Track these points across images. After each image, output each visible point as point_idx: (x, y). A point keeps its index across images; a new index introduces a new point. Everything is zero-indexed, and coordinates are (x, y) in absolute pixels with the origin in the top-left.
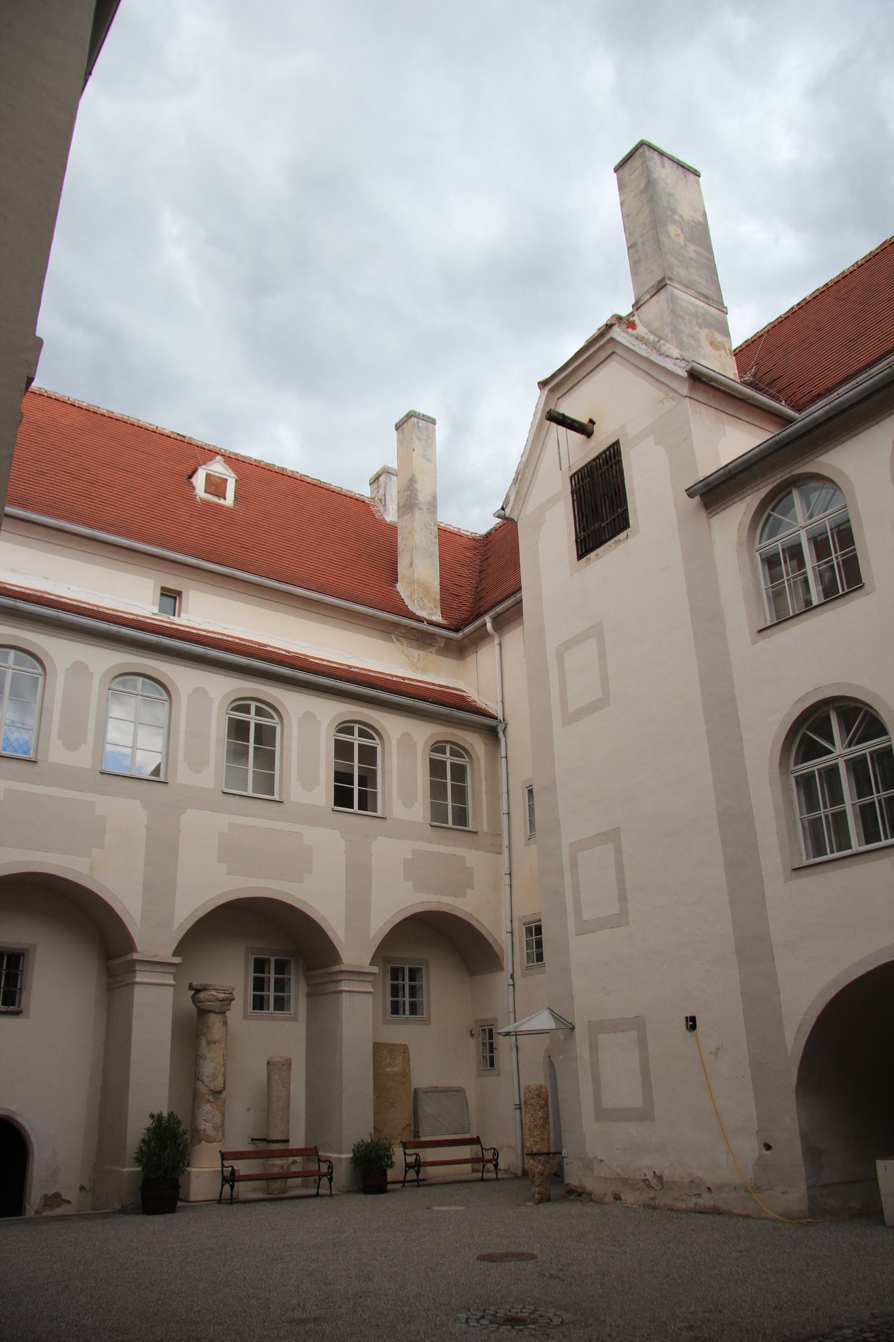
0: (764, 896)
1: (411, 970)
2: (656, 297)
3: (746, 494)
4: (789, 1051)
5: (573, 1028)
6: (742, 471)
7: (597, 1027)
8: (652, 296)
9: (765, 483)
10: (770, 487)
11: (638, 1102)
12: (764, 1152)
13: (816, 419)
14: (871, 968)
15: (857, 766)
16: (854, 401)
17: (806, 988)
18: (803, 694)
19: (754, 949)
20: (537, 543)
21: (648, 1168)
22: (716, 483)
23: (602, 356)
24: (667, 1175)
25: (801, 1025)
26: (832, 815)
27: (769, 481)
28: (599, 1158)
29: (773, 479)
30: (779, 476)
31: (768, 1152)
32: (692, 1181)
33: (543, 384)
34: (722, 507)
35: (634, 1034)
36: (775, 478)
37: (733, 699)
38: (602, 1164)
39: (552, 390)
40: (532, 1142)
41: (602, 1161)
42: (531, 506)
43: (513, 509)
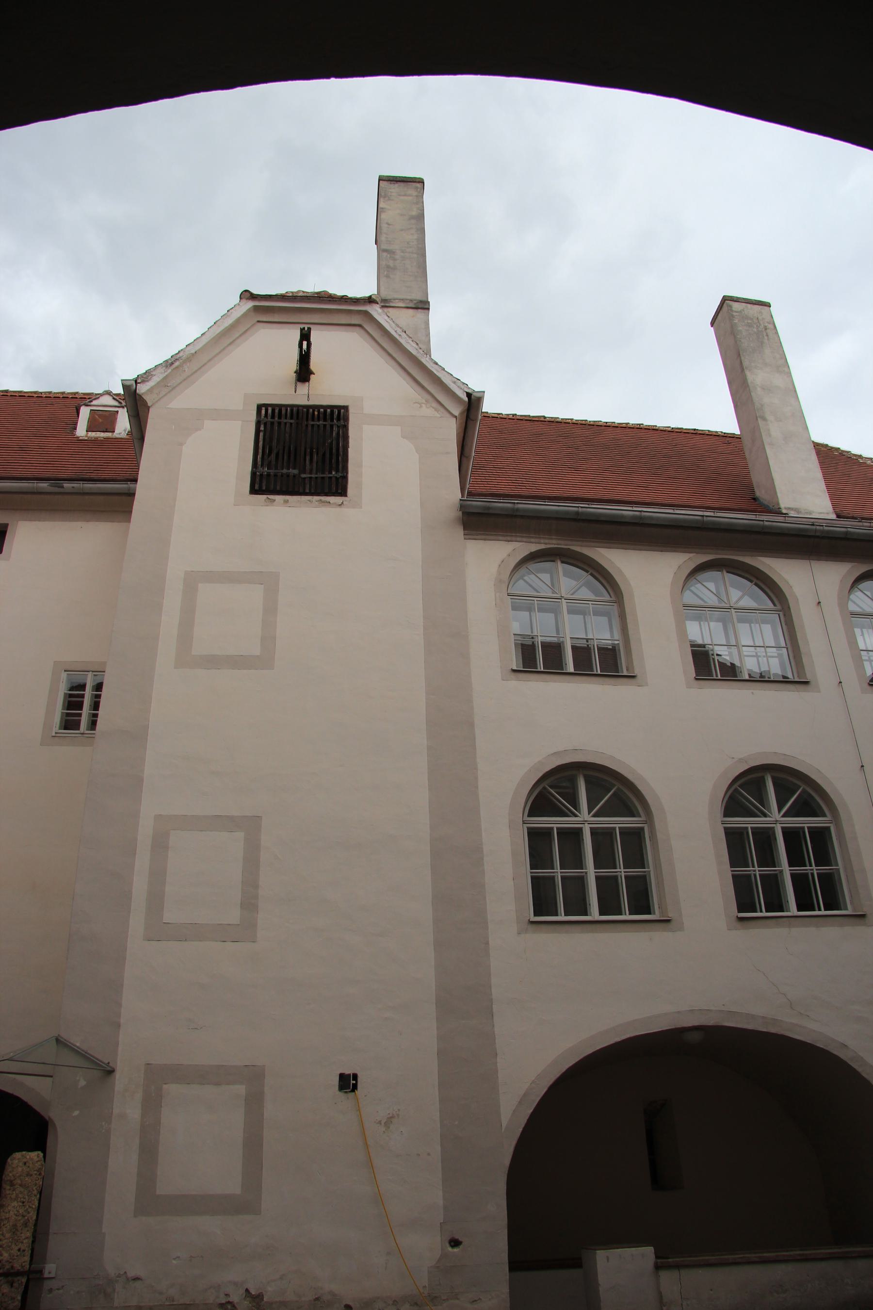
0: (487, 943)
1: (634, 898)
2: (411, 311)
3: (514, 538)
4: (504, 1125)
5: (110, 1072)
6: (522, 517)
7: (158, 1078)
8: (408, 308)
9: (537, 540)
10: (543, 547)
11: (233, 1186)
12: (450, 1249)
13: (623, 516)
14: (618, 1039)
15: (602, 837)
16: (603, 519)
17: (532, 1054)
18: (561, 749)
19: (464, 1003)
20: (182, 444)
21: (235, 1284)
22: (627, 520)
23: (344, 319)
24: (270, 1294)
25: (525, 1095)
26: (554, 877)
27: (542, 541)
28: (131, 1274)
29: (547, 541)
30: (554, 542)
31: (456, 1250)
32: (317, 1299)
33: (247, 295)
34: (483, 537)
35: (241, 1089)
36: (550, 541)
37: (472, 725)
38: (138, 1284)
39: (256, 309)
40: (15, 1251)
41: (137, 1279)
42: (185, 400)
43: (151, 390)
